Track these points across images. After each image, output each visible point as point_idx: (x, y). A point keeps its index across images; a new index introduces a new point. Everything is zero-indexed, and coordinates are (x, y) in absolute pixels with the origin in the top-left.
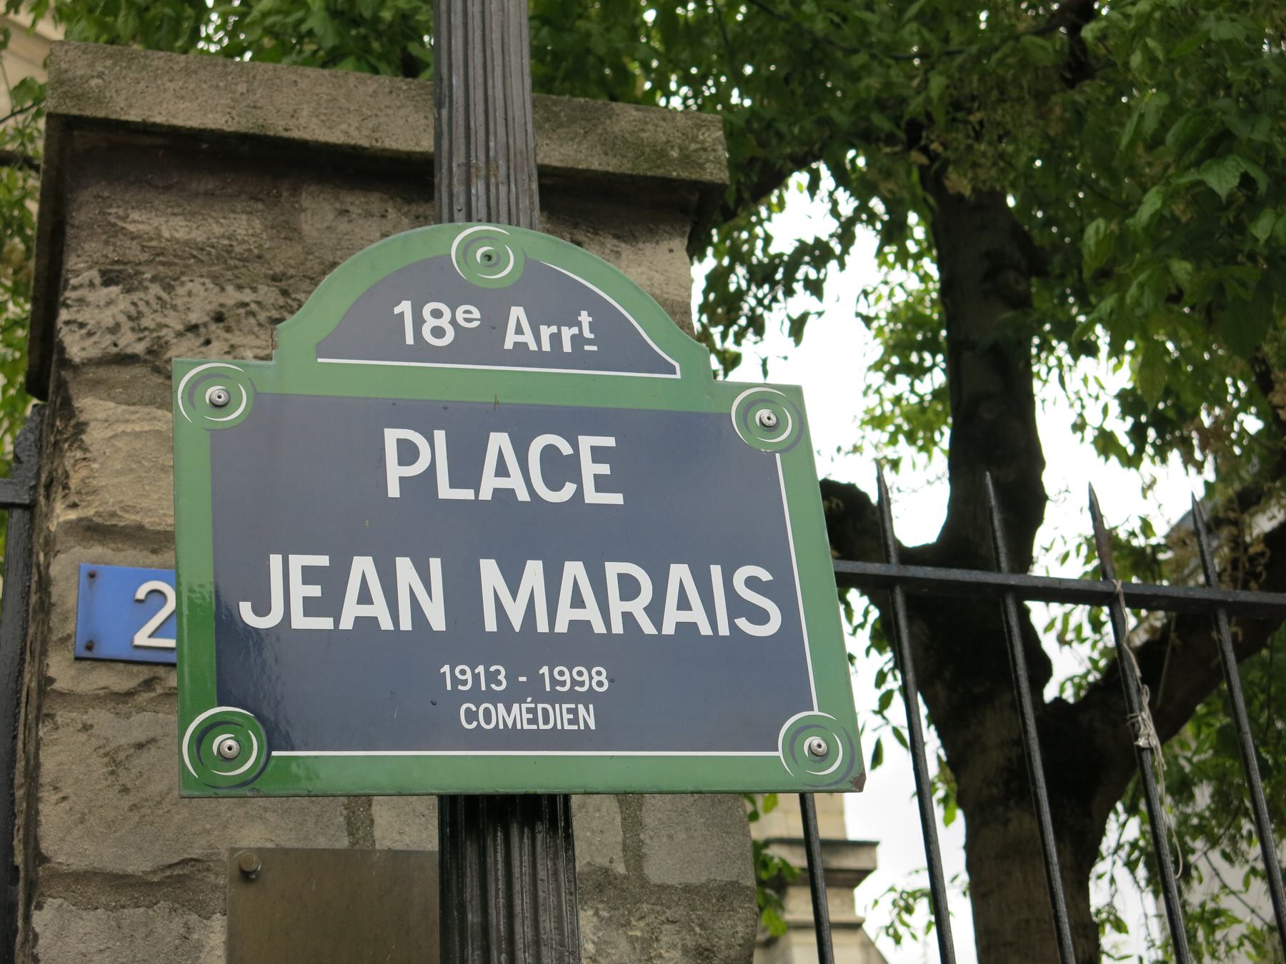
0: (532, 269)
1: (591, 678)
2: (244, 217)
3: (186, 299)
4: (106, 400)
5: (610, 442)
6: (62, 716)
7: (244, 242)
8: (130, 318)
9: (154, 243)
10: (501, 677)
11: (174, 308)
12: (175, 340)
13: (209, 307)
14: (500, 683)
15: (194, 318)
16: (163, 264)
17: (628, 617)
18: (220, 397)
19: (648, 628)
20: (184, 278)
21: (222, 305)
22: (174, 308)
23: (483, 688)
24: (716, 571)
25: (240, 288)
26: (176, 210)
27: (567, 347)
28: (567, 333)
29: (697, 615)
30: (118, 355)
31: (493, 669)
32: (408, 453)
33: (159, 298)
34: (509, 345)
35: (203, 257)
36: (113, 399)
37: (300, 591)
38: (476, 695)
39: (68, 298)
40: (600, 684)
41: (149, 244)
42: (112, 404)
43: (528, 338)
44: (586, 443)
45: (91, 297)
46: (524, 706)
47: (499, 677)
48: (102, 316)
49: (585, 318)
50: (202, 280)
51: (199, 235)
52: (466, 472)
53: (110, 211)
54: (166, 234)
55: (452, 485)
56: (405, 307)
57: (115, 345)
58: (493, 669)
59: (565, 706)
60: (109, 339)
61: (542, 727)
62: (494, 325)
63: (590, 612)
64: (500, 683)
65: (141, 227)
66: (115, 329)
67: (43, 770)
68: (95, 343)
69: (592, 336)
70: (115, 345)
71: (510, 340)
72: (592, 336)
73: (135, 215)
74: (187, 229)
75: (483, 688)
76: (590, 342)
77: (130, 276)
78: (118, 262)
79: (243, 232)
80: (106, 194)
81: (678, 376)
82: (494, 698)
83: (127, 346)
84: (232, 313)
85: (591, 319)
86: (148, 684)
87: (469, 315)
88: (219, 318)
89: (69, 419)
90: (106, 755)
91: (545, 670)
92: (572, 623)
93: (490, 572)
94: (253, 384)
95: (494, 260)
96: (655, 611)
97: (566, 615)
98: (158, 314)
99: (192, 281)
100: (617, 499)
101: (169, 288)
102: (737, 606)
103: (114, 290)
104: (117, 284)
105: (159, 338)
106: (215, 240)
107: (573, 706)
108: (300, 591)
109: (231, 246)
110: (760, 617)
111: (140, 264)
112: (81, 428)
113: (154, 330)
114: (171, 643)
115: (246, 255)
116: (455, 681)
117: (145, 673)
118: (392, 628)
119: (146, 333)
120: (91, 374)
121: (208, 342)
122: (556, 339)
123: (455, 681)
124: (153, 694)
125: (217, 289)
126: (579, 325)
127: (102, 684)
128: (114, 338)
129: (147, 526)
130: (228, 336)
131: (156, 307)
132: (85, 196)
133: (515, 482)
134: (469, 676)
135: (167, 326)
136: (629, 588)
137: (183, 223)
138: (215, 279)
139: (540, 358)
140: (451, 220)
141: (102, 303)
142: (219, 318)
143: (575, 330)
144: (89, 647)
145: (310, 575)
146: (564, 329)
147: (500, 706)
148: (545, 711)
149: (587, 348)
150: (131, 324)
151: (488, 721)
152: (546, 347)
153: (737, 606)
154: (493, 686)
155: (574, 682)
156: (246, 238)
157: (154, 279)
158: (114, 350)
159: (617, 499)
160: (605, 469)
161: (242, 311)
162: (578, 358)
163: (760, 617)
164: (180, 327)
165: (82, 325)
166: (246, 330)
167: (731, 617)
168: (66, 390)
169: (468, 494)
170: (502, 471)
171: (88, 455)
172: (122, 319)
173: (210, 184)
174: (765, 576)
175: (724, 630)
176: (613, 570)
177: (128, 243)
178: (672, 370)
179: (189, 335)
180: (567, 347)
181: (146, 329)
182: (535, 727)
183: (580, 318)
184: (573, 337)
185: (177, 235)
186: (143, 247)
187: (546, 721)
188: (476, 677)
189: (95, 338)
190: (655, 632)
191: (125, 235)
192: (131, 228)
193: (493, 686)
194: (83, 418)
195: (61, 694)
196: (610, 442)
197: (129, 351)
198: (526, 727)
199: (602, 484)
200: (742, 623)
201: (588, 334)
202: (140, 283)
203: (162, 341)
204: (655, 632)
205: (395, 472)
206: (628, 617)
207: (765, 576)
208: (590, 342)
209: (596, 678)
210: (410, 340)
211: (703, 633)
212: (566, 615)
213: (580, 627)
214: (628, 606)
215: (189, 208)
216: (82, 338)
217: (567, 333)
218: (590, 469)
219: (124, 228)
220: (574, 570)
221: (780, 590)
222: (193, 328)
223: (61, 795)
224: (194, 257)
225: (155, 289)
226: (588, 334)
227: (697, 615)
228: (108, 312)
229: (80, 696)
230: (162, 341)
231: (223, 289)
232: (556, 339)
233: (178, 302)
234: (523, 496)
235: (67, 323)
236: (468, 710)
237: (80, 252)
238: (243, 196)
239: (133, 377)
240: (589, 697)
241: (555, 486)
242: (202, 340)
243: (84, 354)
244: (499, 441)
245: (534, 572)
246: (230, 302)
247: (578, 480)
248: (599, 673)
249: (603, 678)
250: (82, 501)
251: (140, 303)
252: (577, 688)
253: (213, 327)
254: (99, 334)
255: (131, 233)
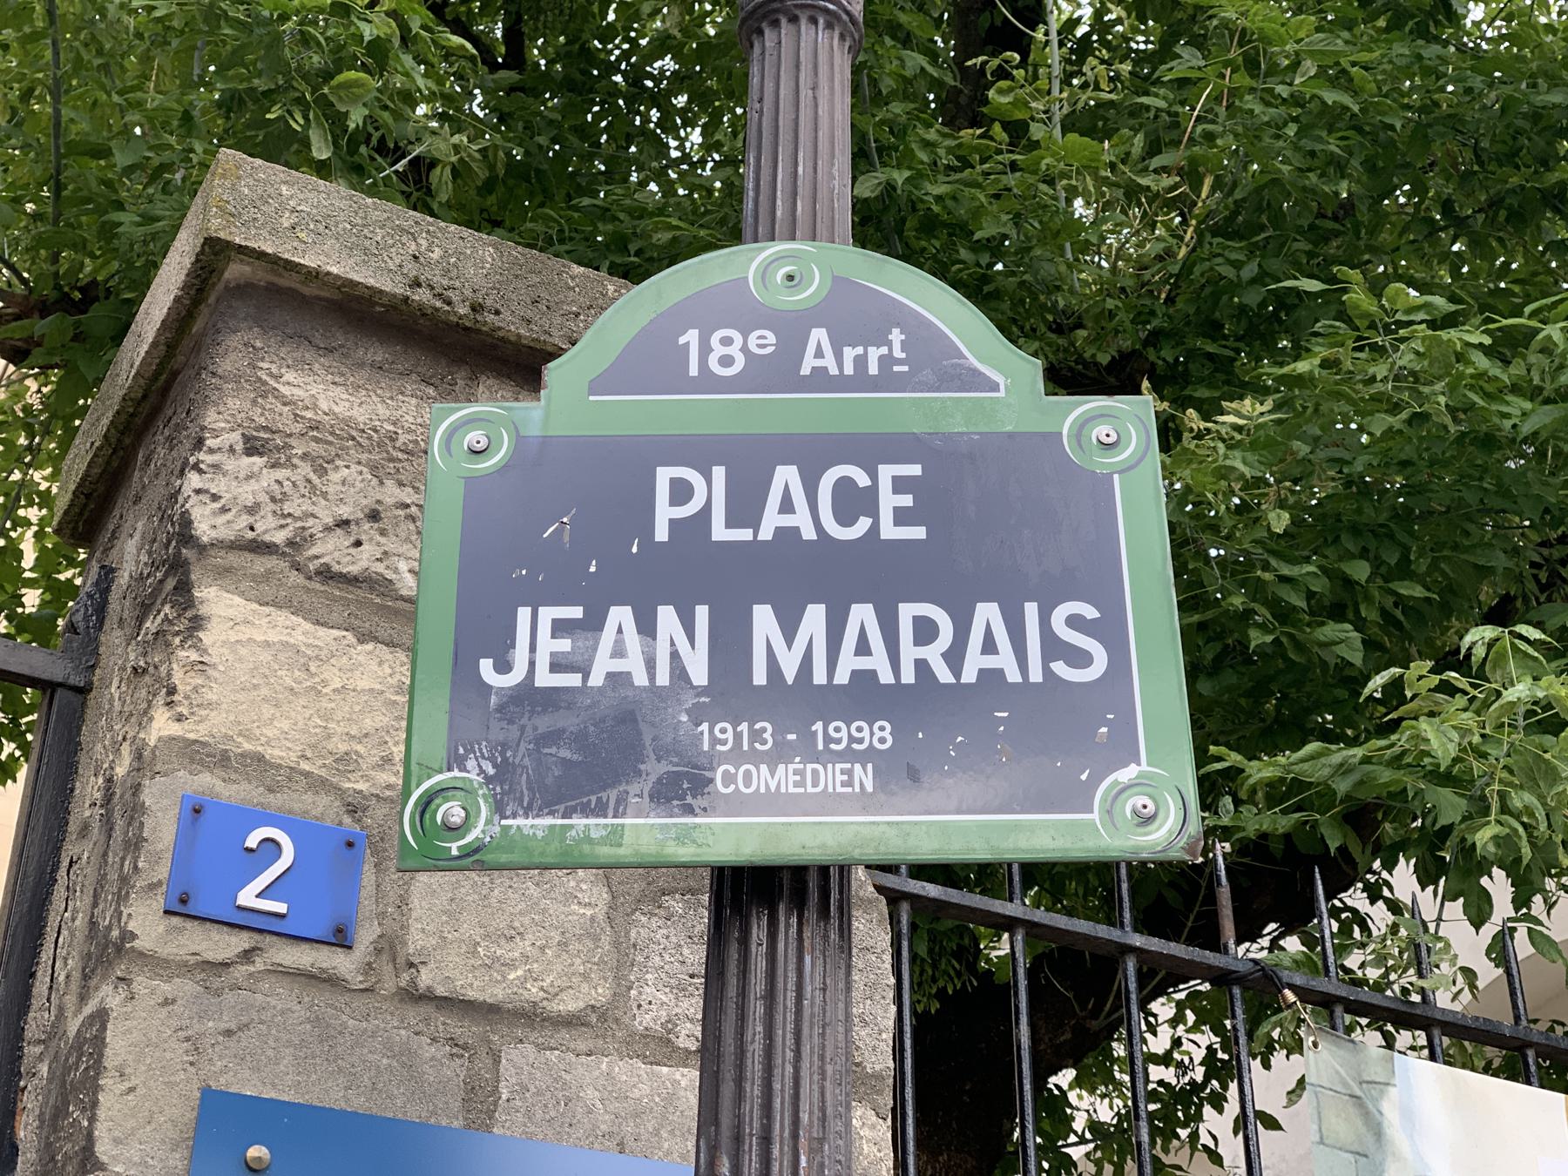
0: (841, 285)
1: (872, 734)
2: (414, 401)
3: (339, 488)
4: (233, 593)
5: (915, 470)
6: (141, 984)
7: (410, 431)
8: (273, 500)
9: (309, 414)
10: (767, 736)
11: (324, 495)
12: (320, 535)
13: (365, 502)
14: (764, 742)
15: (345, 512)
16: (317, 440)
17: (922, 666)
18: (478, 442)
19: (944, 675)
20: (338, 462)
21: (378, 502)
22: (324, 495)
23: (746, 748)
24: (1031, 610)
25: (401, 484)
26: (337, 380)
27: (873, 369)
28: (874, 354)
29: (1005, 660)
30: (254, 540)
31: (757, 726)
32: (681, 492)
33: (309, 481)
34: (805, 370)
35: (365, 442)
36: (242, 594)
37: (549, 645)
38: (737, 755)
39: (203, 462)
40: (882, 740)
41: (303, 413)
42: (238, 600)
43: (829, 361)
44: (886, 472)
45: (230, 464)
46: (791, 767)
47: (765, 735)
48: (240, 490)
49: (896, 336)
50: (360, 468)
51: (361, 415)
52: (744, 509)
53: (261, 364)
54: (324, 405)
55: (729, 525)
56: (691, 337)
57: (252, 529)
58: (757, 726)
59: (839, 766)
60: (245, 520)
61: (810, 789)
62: (793, 345)
63: (878, 662)
64: (764, 742)
65: (296, 391)
66: (252, 510)
67: (108, 1052)
68: (228, 522)
69: (903, 355)
70: (252, 529)
71: (808, 364)
72: (903, 355)
73: (290, 376)
74: (347, 404)
75: (746, 748)
76: (900, 362)
77: (278, 449)
78: (266, 429)
79: (411, 420)
80: (258, 344)
81: (1002, 394)
82: (756, 758)
83: (266, 532)
84: (389, 514)
85: (903, 337)
86: (247, 955)
87: (764, 341)
88: (374, 516)
89: (185, 609)
90: (188, 1039)
91: (818, 727)
92: (854, 673)
93: (764, 619)
94: (516, 428)
95: (795, 282)
96: (954, 656)
97: (848, 663)
98: (306, 499)
99: (347, 467)
100: (919, 533)
101: (321, 471)
102: (1053, 647)
103: (258, 461)
104: (261, 454)
105: (304, 528)
106: (377, 423)
107: (849, 765)
108: (549, 645)
109: (396, 433)
110: (1080, 658)
111: (290, 435)
112: (197, 623)
113: (300, 519)
114: (281, 908)
115: (411, 446)
116: (715, 741)
117: (242, 941)
118: (647, 683)
119: (289, 520)
120: (220, 559)
121: (358, 544)
122: (861, 362)
123: (715, 741)
124: (252, 969)
125: (375, 481)
126: (890, 344)
127: (195, 949)
128: (251, 520)
129: (268, 757)
130: (382, 540)
131: (303, 491)
132: (234, 341)
133: (801, 520)
134: (730, 735)
135: (314, 516)
136: (925, 631)
137: (345, 396)
138: (374, 468)
139: (841, 383)
140: (756, 241)
141: (242, 475)
142: (374, 516)
143: (884, 350)
144: (184, 902)
145: (560, 628)
146: (871, 350)
147: (764, 768)
148: (815, 772)
149: (896, 369)
150: (272, 506)
151: (748, 784)
152: (849, 370)
153: (1053, 647)
154: (757, 745)
155: (852, 739)
156: (413, 427)
157: (305, 457)
158: (250, 535)
159: (919, 533)
160: (907, 500)
161: (401, 512)
162: (887, 380)
163: (1080, 658)
164: (329, 521)
165: (215, 498)
166: (403, 535)
167: (1047, 658)
168: (187, 573)
169: (745, 535)
170: (787, 506)
171: (205, 659)
172: (263, 498)
173: (378, 354)
174: (1090, 612)
175: (1036, 676)
176: (907, 612)
177: (279, 407)
178: (995, 387)
179: (339, 531)
180: (873, 369)
181: (290, 515)
182: (802, 790)
183: (890, 337)
184: (881, 358)
185: (336, 409)
186: (296, 415)
187: (815, 784)
188: (738, 736)
189: (229, 516)
190: (953, 681)
191: (276, 398)
192: (285, 390)
193: (757, 745)
194: (203, 610)
195: (141, 954)
196: (915, 470)
197: (267, 538)
198: (792, 790)
199: (901, 516)
200: (1059, 668)
201: (898, 353)
202: (289, 459)
203: (307, 533)
204: (953, 681)
205: (665, 513)
206: (922, 666)
207: (1090, 612)
208: (900, 362)
209: (878, 734)
210: (694, 371)
211: (1010, 680)
212: (848, 663)
213: (864, 678)
214: (923, 652)
215: (352, 379)
216: (214, 513)
217: (874, 354)
218: (889, 501)
219: (275, 389)
220: (862, 615)
221: (1110, 630)
222: (343, 524)
223: (127, 1085)
224: (353, 439)
225: (305, 469)
226: (898, 353)
227: (1005, 660)
228: (253, 485)
229: (166, 961)
230: (307, 533)
231: (381, 483)
232: (861, 362)
233: (331, 489)
234: (809, 533)
235: (198, 492)
236: (726, 772)
237: (222, 409)
238: (414, 376)
239: (269, 572)
240: (869, 755)
241: (845, 519)
242: (352, 539)
243: (214, 534)
244: (787, 476)
245: (815, 618)
246: (389, 501)
247: (874, 514)
248: (882, 729)
249: (887, 734)
250: (192, 713)
251: (286, 483)
252: (855, 746)
253: (367, 526)
254: (234, 511)
255: (284, 396)
